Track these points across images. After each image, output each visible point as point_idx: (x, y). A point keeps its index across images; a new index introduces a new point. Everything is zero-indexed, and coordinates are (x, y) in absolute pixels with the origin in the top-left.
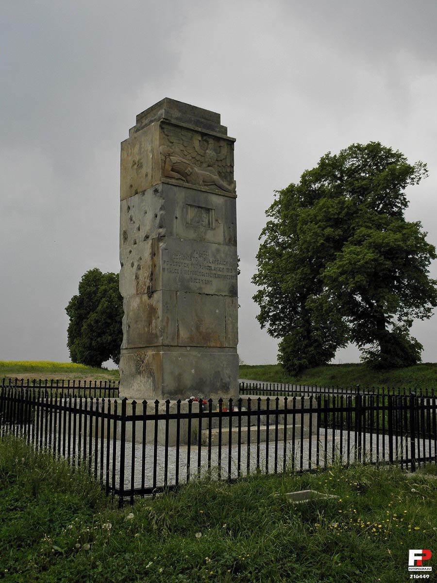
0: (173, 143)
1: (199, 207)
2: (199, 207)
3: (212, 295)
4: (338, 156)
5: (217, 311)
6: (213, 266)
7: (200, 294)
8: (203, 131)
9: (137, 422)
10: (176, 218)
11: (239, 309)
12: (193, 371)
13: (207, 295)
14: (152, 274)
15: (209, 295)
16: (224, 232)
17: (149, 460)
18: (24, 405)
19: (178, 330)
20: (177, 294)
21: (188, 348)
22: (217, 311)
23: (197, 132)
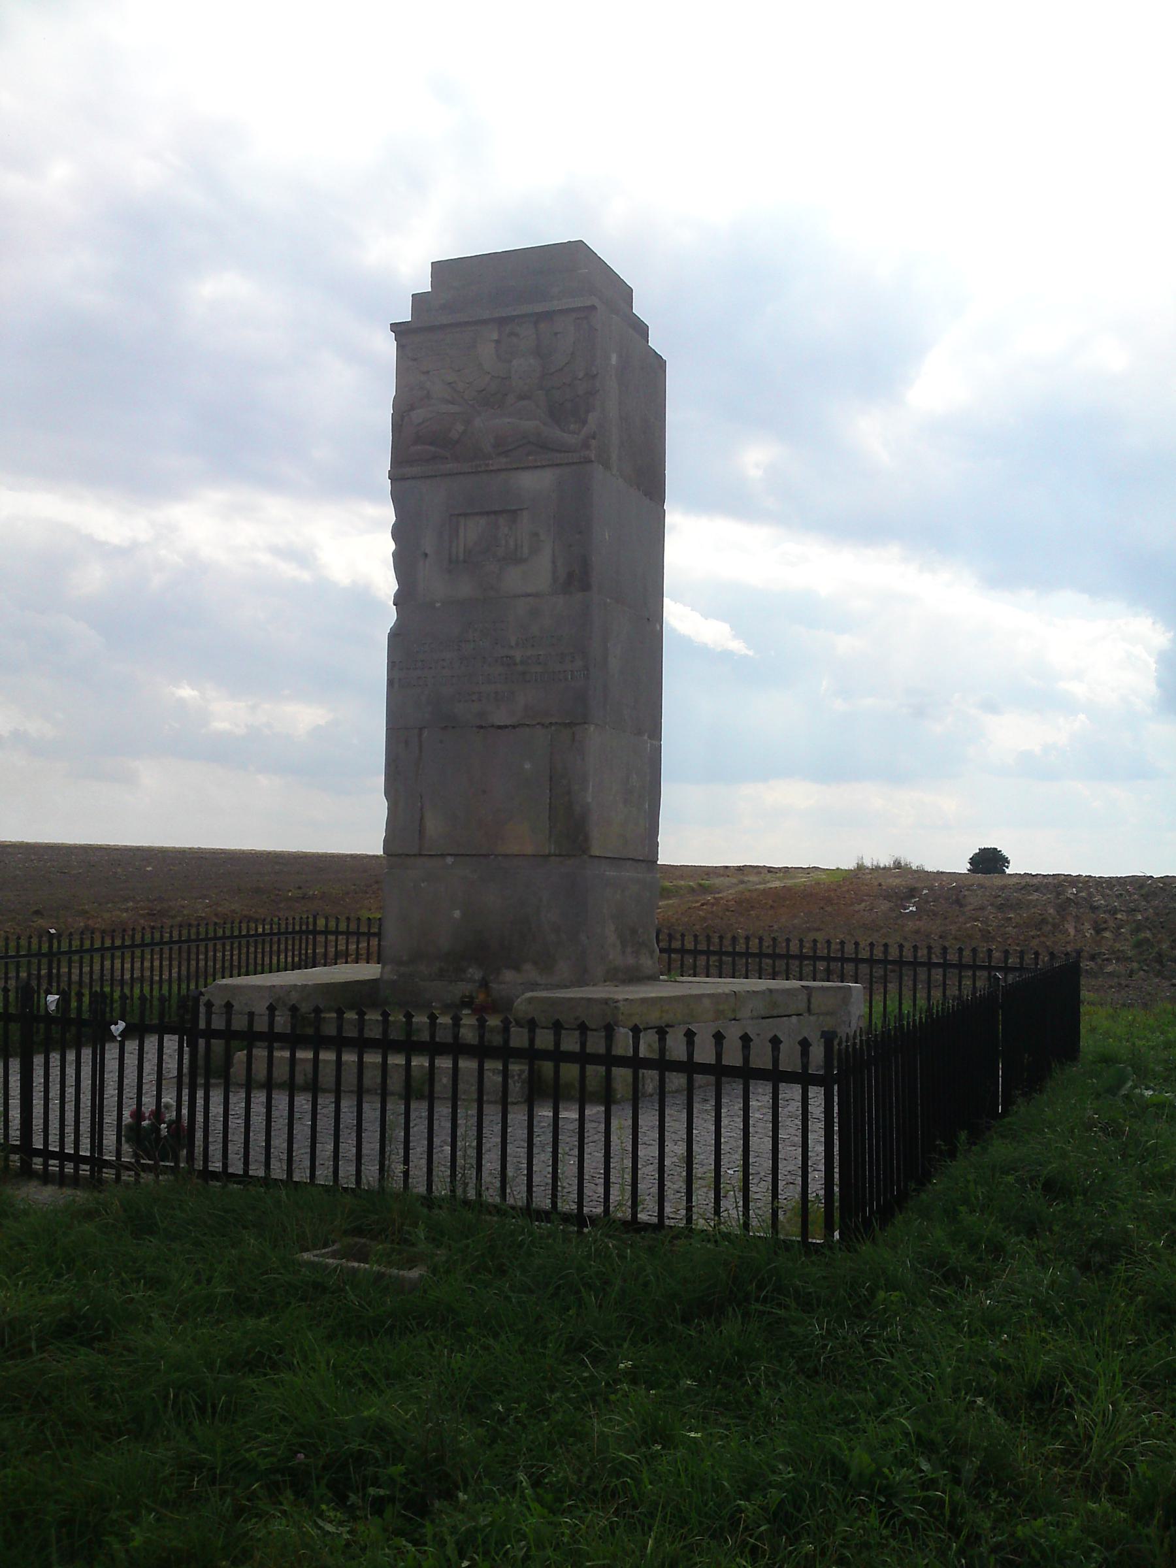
0: (428, 372)
1: (488, 513)
2: (488, 513)
3: (514, 727)
4: (939, 386)
5: (527, 766)
6: (518, 655)
7: (481, 727)
8: (497, 315)
9: (166, 1037)
10: (426, 555)
11: (868, 863)
12: (457, 914)
13: (499, 727)
14: (551, 777)
15: (506, 727)
16: (554, 562)
17: (258, 1121)
18: (836, 1087)
19: (422, 819)
20: (420, 735)
21: (450, 860)
22: (527, 766)
23: (484, 322)
